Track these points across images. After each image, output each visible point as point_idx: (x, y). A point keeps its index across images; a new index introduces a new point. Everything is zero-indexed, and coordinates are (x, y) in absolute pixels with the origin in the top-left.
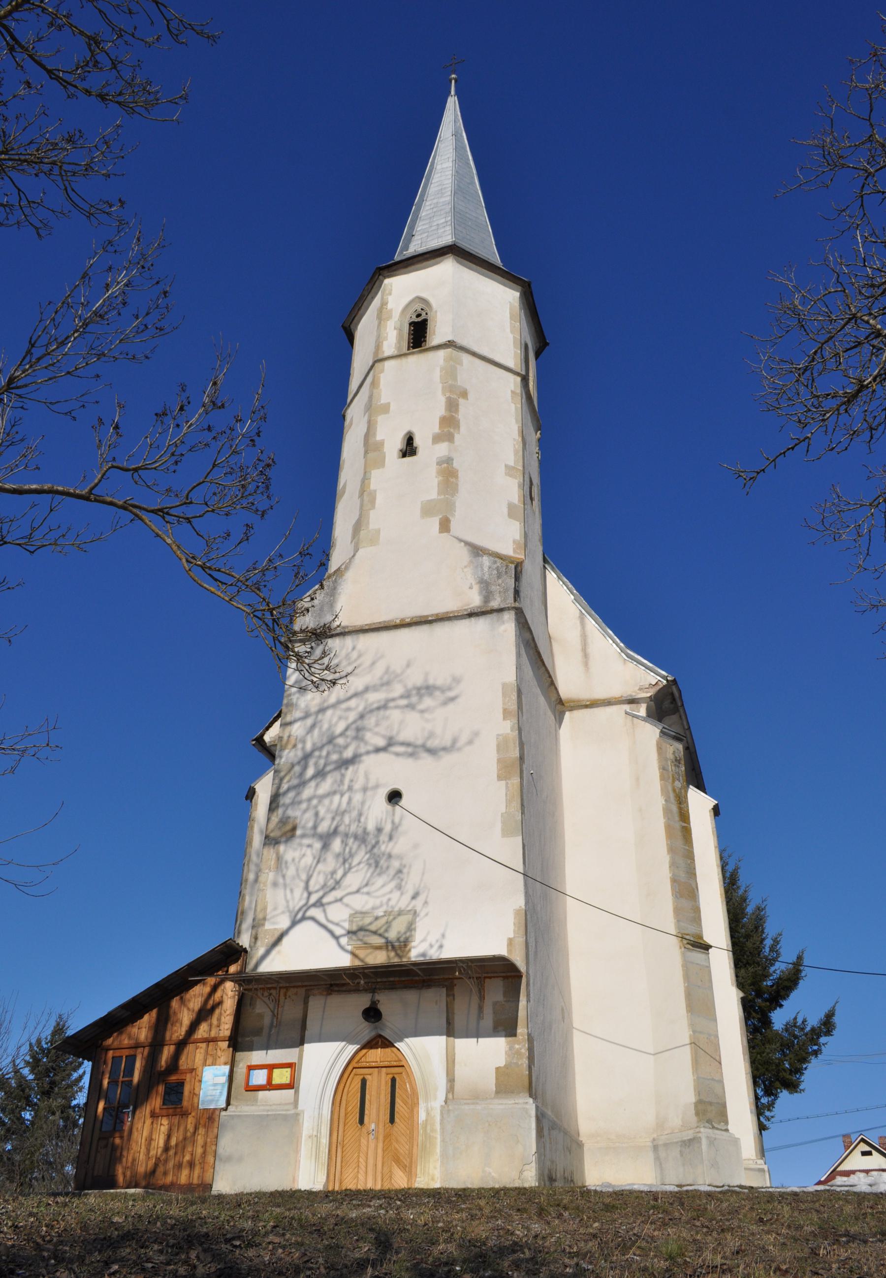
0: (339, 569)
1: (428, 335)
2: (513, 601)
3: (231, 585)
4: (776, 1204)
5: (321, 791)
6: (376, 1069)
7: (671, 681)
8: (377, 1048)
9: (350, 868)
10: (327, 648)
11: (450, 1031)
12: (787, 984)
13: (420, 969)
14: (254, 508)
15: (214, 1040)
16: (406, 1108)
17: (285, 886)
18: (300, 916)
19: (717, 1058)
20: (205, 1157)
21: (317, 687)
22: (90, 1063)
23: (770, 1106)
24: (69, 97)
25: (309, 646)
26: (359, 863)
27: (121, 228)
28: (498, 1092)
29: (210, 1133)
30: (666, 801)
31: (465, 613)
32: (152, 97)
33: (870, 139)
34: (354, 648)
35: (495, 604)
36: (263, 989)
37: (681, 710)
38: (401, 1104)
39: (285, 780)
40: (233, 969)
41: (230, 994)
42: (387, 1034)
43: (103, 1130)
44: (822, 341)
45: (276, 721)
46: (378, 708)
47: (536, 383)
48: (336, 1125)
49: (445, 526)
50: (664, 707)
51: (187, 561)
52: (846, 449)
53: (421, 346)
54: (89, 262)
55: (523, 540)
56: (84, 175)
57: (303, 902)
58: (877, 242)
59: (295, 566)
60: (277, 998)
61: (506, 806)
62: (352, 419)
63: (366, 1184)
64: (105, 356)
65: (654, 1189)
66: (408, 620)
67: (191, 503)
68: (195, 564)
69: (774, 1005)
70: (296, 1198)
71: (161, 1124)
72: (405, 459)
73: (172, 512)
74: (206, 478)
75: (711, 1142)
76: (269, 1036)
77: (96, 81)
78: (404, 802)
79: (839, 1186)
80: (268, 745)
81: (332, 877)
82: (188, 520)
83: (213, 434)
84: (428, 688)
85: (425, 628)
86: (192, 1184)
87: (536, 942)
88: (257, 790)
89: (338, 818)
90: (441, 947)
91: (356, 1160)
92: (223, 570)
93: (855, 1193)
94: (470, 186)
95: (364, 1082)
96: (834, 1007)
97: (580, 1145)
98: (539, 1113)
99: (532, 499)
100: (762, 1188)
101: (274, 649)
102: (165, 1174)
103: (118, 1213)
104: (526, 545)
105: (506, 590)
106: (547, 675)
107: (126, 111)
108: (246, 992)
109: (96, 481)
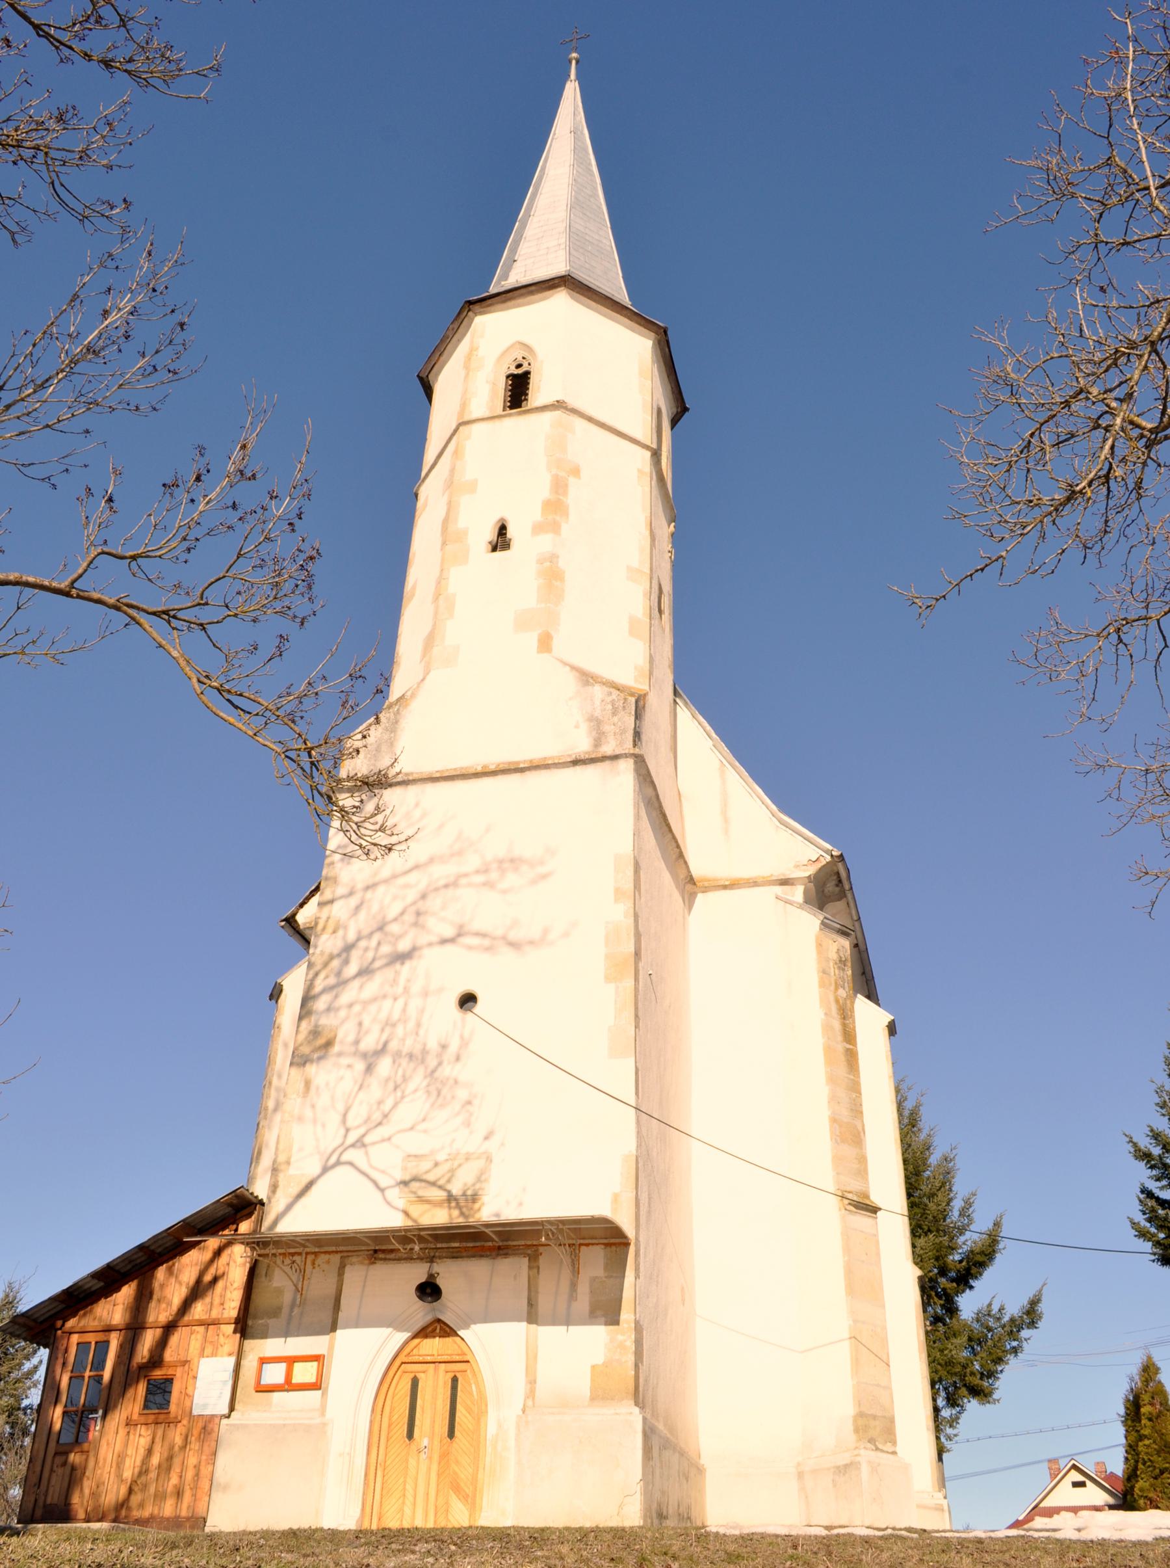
0: (403, 697)
1: (530, 392)
2: (632, 746)
3: (257, 714)
4: (953, 1554)
6: (432, 1365)
7: (837, 857)
8: (434, 1337)
9: (403, 1097)
10: (381, 802)
11: (532, 1316)
12: (980, 1258)
13: (494, 1232)
14: (290, 613)
15: (216, 1323)
16: (470, 1418)
17: (315, 1121)
19: (885, 1358)
20: (198, 1480)
21: (367, 854)
22: (47, 1350)
23: (953, 1422)
24: (62, 61)
25: (359, 799)
26: (415, 1091)
27: (125, 237)
28: (593, 1398)
29: (206, 1448)
30: (826, 1014)
31: (569, 760)
32: (173, 67)
33: (1109, 162)
34: (417, 805)
35: (608, 749)
36: (284, 1254)
37: (849, 895)
39: (322, 976)
40: (245, 1227)
41: (240, 1260)
42: (447, 1318)
43: (61, 1442)
44: (1042, 421)
45: (313, 896)
46: (446, 886)
47: (670, 460)
48: (375, 1439)
49: (545, 643)
50: (826, 890)
51: (199, 681)
52: (1053, 572)
53: (520, 406)
54: (81, 280)
55: (648, 665)
56: (77, 165)
57: (339, 1141)
58: (1097, 306)
59: (342, 691)
60: (302, 1267)
61: (615, 1017)
62: (426, 501)
63: (413, 1517)
64: (98, 405)
65: (794, 1533)
66: (492, 767)
67: (207, 604)
68: (209, 686)
69: (962, 1287)
70: (315, 1540)
71: (140, 1435)
72: (495, 553)
73: (180, 615)
74: (227, 572)
76: (290, 1317)
77: (99, 42)
78: (479, 1008)
79: (1037, 1530)
80: (301, 927)
81: (378, 1108)
82: (202, 626)
83: (240, 513)
84: (512, 861)
86: (179, 1517)
87: (650, 1199)
88: (284, 988)
89: (388, 1031)
90: (520, 1204)
91: (401, 1488)
92: (247, 695)
93: (1057, 1540)
94: (592, 199)
95: (415, 1383)
96: (1040, 1291)
97: (701, 1471)
98: (647, 1429)
99: (660, 611)
100: (938, 1531)
101: (311, 801)
102: (141, 1505)
103: (70, 1560)
104: (651, 673)
105: (623, 732)
106: (674, 845)
107: (138, 82)
108: (261, 1259)
109: (80, 571)
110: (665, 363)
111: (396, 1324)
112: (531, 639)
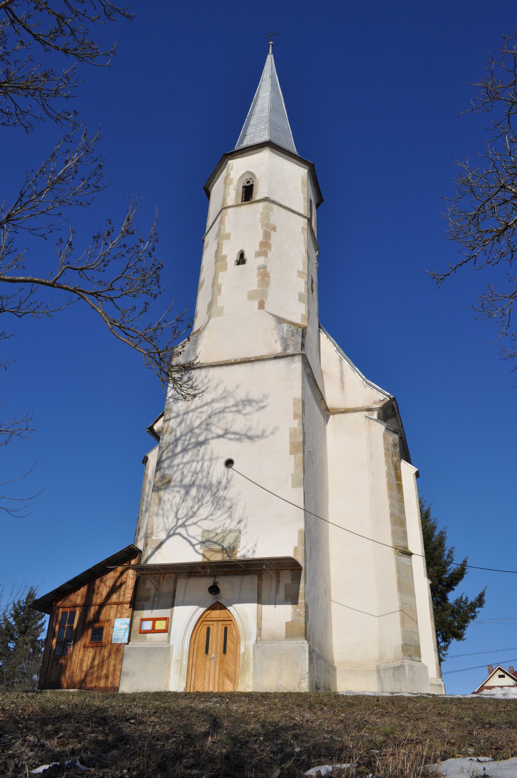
5: (185, 460)
11: (260, 601)
15: (122, 603)
18: (172, 532)
34: (206, 377)
35: (290, 351)
38: (230, 642)
42: (222, 601)
46: (219, 412)
49: (262, 305)
57: (174, 524)
66: (239, 360)
75: (411, 668)
76: (154, 601)
85: (249, 365)
95: (208, 629)
96: (484, 591)
97: (334, 668)
105: (297, 344)
110: (313, 180)
111: (200, 604)
112: (255, 304)
